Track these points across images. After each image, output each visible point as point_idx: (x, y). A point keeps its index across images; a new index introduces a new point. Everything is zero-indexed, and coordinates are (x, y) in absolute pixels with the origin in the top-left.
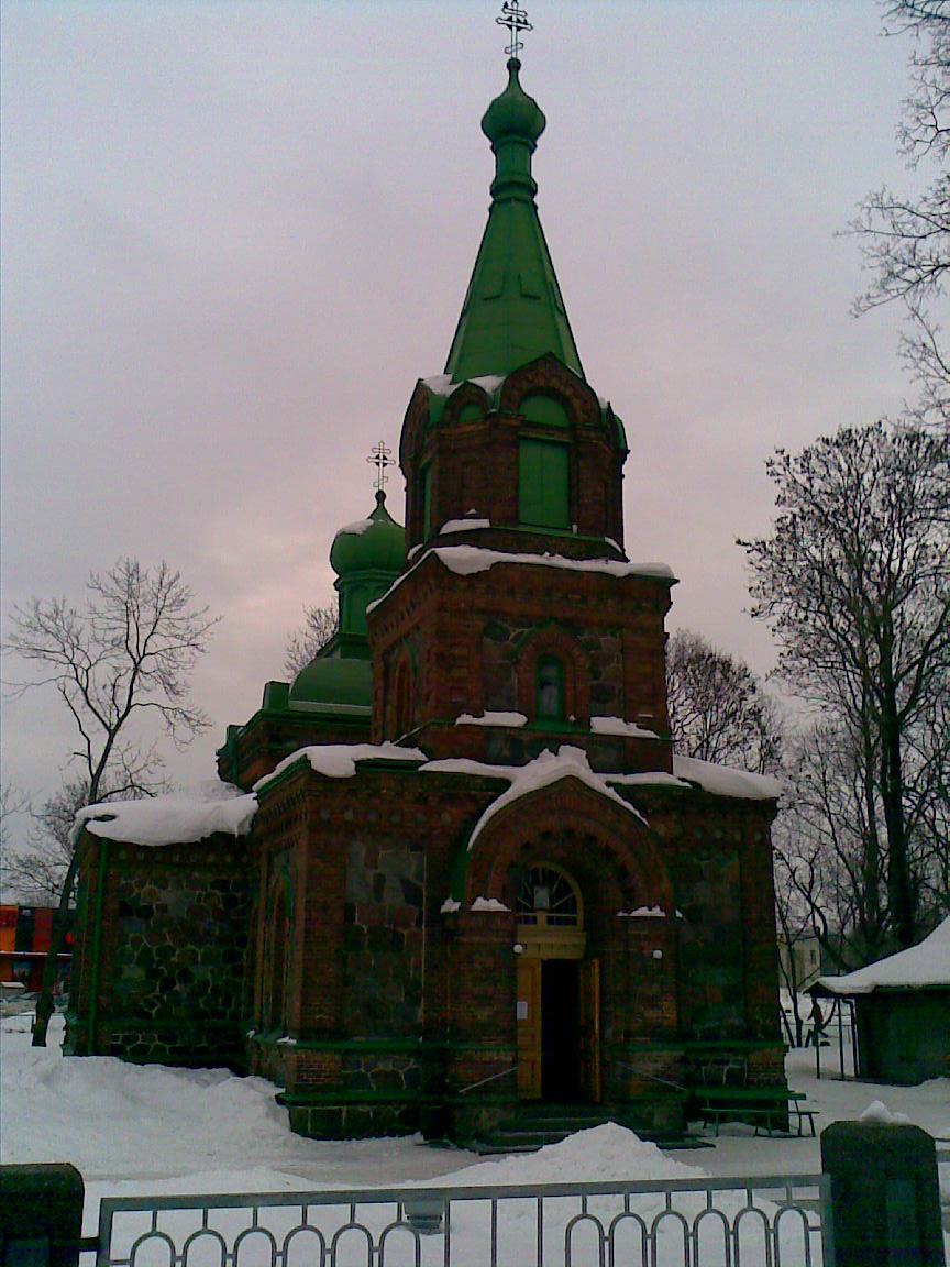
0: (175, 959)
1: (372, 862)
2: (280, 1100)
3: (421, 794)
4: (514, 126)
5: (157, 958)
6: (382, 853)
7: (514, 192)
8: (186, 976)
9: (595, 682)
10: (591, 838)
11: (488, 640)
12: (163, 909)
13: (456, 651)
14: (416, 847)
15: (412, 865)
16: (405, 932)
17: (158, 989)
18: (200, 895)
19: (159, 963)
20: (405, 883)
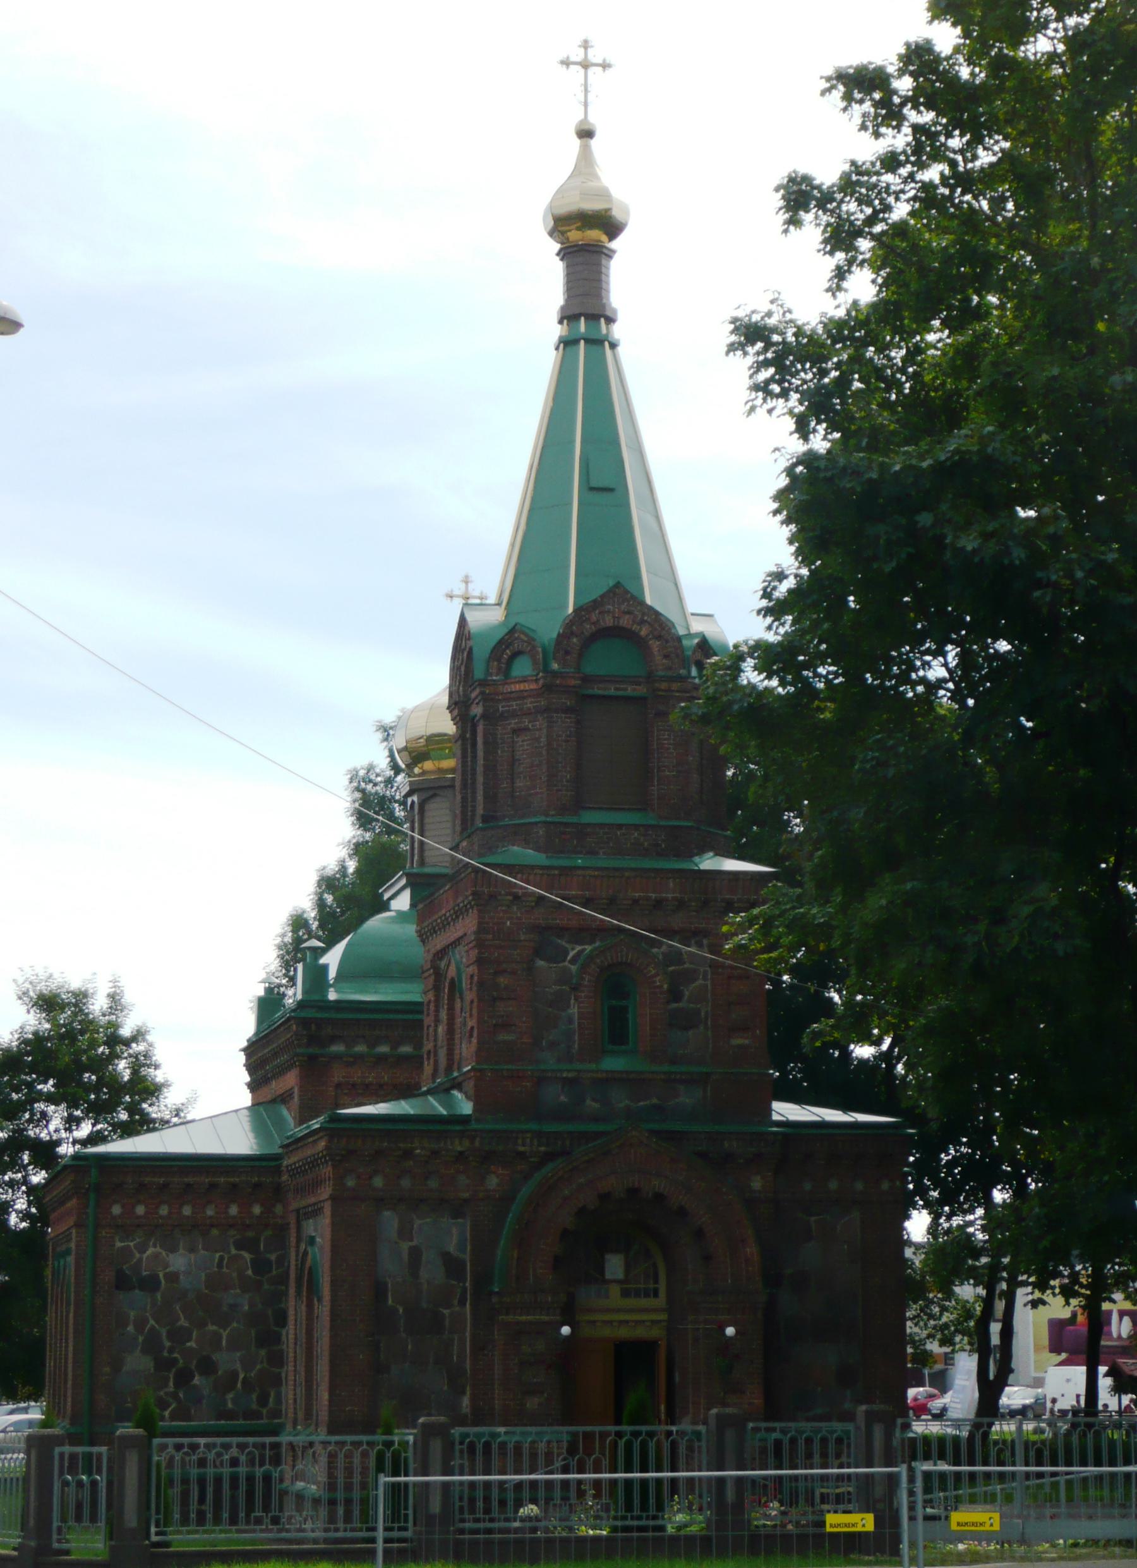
0: (192, 1344)
1: (405, 1232)
2: (157, 1067)
3: (461, 1153)
4: (586, 236)
5: (168, 1344)
6: (417, 1223)
7: (586, 315)
8: (207, 1367)
9: (675, 1005)
10: (660, 1197)
11: (541, 963)
12: (173, 1277)
13: (502, 980)
14: (457, 1213)
15: (454, 1236)
16: (446, 1312)
17: (171, 1384)
18: (221, 1259)
19: (171, 1351)
20: (447, 1258)
